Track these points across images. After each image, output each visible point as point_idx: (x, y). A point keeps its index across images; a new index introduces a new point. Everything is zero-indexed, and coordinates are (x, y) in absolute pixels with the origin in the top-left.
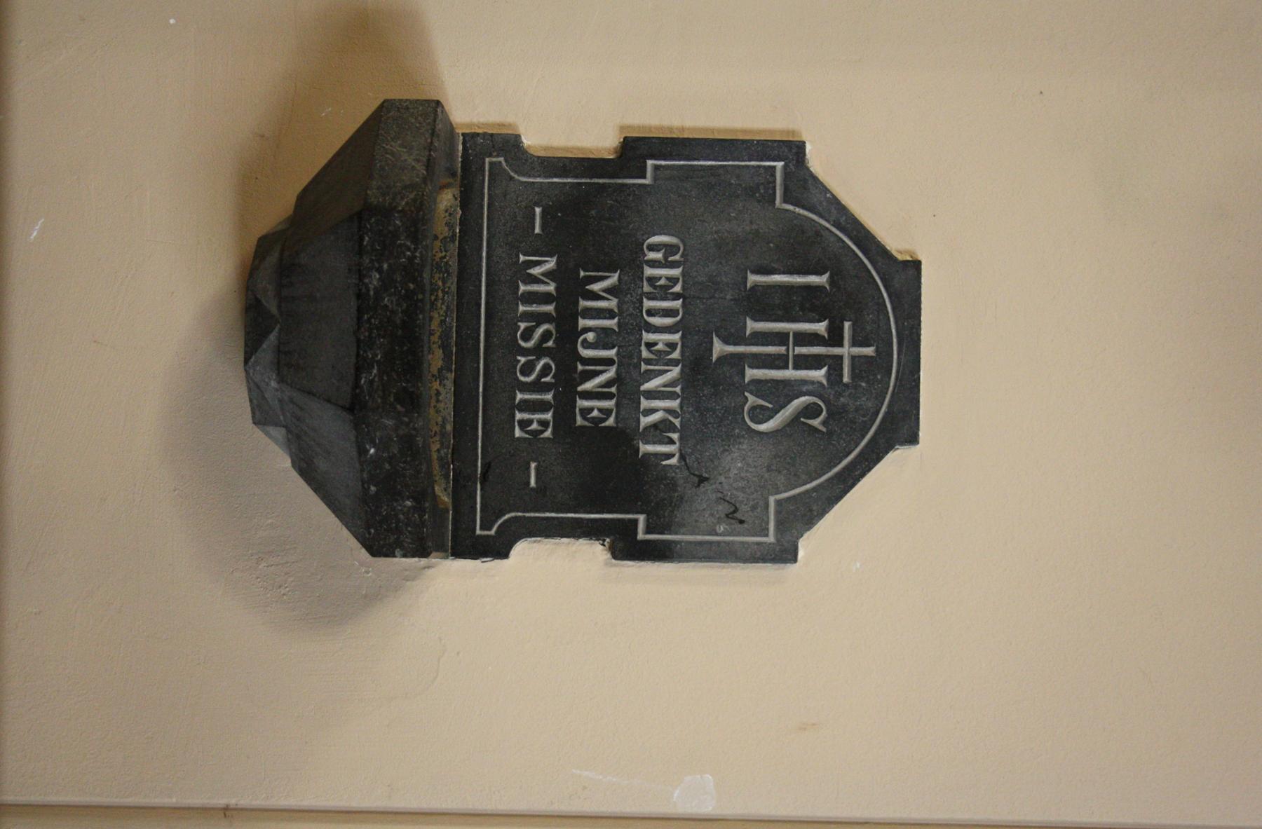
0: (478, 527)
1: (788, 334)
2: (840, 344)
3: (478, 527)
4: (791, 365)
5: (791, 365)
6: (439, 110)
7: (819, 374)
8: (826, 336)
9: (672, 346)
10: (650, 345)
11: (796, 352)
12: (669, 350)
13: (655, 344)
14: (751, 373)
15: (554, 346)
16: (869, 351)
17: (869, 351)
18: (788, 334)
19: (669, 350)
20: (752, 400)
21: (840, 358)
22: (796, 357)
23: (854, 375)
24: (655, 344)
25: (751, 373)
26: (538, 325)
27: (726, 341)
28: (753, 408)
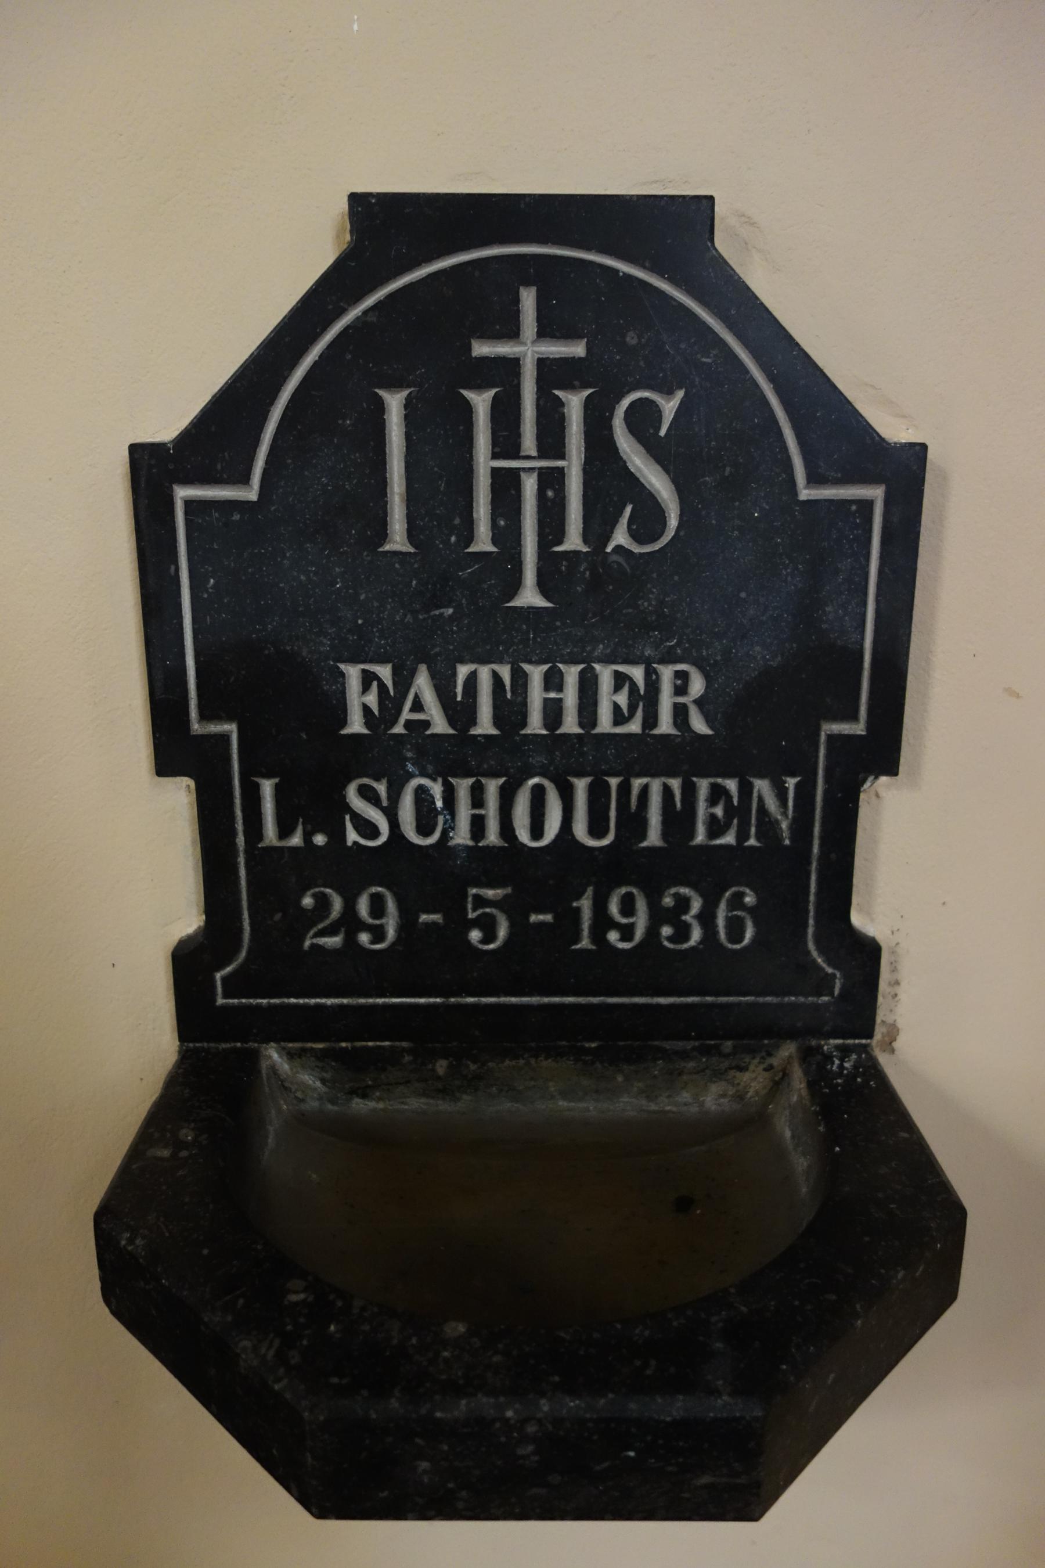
0: (194, 713)
1: (562, 456)
2: (513, 365)
3: (194, 713)
4: (560, 463)
5: (560, 463)
6: (287, 1084)
7: (574, 403)
8: (493, 392)
9: (620, 680)
10: (619, 717)
11: (534, 453)
12: (627, 685)
13: (616, 707)
14: (573, 541)
15: (384, 781)
16: (528, 299)
17: (528, 299)
18: (562, 456)
19: (627, 685)
20: (621, 537)
21: (542, 363)
22: (542, 454)
23: (568, 334)
24: (616, 707)
25: (573, 541)
26: (384, 810)
27: (515, 585)
28: (635, 535)
